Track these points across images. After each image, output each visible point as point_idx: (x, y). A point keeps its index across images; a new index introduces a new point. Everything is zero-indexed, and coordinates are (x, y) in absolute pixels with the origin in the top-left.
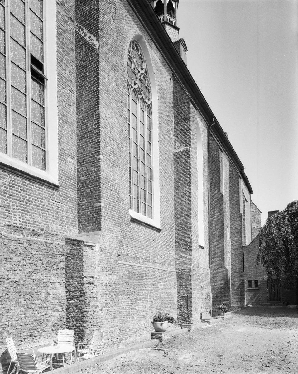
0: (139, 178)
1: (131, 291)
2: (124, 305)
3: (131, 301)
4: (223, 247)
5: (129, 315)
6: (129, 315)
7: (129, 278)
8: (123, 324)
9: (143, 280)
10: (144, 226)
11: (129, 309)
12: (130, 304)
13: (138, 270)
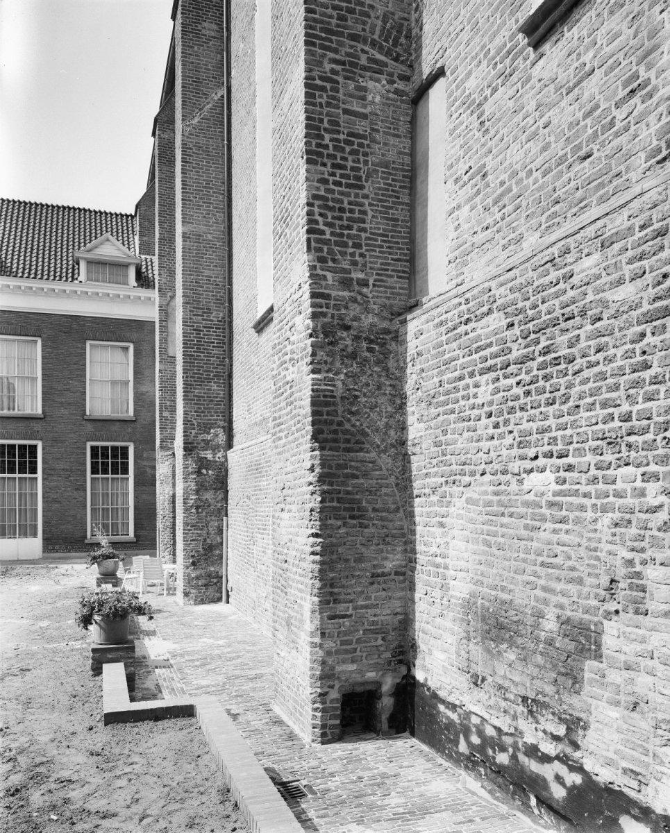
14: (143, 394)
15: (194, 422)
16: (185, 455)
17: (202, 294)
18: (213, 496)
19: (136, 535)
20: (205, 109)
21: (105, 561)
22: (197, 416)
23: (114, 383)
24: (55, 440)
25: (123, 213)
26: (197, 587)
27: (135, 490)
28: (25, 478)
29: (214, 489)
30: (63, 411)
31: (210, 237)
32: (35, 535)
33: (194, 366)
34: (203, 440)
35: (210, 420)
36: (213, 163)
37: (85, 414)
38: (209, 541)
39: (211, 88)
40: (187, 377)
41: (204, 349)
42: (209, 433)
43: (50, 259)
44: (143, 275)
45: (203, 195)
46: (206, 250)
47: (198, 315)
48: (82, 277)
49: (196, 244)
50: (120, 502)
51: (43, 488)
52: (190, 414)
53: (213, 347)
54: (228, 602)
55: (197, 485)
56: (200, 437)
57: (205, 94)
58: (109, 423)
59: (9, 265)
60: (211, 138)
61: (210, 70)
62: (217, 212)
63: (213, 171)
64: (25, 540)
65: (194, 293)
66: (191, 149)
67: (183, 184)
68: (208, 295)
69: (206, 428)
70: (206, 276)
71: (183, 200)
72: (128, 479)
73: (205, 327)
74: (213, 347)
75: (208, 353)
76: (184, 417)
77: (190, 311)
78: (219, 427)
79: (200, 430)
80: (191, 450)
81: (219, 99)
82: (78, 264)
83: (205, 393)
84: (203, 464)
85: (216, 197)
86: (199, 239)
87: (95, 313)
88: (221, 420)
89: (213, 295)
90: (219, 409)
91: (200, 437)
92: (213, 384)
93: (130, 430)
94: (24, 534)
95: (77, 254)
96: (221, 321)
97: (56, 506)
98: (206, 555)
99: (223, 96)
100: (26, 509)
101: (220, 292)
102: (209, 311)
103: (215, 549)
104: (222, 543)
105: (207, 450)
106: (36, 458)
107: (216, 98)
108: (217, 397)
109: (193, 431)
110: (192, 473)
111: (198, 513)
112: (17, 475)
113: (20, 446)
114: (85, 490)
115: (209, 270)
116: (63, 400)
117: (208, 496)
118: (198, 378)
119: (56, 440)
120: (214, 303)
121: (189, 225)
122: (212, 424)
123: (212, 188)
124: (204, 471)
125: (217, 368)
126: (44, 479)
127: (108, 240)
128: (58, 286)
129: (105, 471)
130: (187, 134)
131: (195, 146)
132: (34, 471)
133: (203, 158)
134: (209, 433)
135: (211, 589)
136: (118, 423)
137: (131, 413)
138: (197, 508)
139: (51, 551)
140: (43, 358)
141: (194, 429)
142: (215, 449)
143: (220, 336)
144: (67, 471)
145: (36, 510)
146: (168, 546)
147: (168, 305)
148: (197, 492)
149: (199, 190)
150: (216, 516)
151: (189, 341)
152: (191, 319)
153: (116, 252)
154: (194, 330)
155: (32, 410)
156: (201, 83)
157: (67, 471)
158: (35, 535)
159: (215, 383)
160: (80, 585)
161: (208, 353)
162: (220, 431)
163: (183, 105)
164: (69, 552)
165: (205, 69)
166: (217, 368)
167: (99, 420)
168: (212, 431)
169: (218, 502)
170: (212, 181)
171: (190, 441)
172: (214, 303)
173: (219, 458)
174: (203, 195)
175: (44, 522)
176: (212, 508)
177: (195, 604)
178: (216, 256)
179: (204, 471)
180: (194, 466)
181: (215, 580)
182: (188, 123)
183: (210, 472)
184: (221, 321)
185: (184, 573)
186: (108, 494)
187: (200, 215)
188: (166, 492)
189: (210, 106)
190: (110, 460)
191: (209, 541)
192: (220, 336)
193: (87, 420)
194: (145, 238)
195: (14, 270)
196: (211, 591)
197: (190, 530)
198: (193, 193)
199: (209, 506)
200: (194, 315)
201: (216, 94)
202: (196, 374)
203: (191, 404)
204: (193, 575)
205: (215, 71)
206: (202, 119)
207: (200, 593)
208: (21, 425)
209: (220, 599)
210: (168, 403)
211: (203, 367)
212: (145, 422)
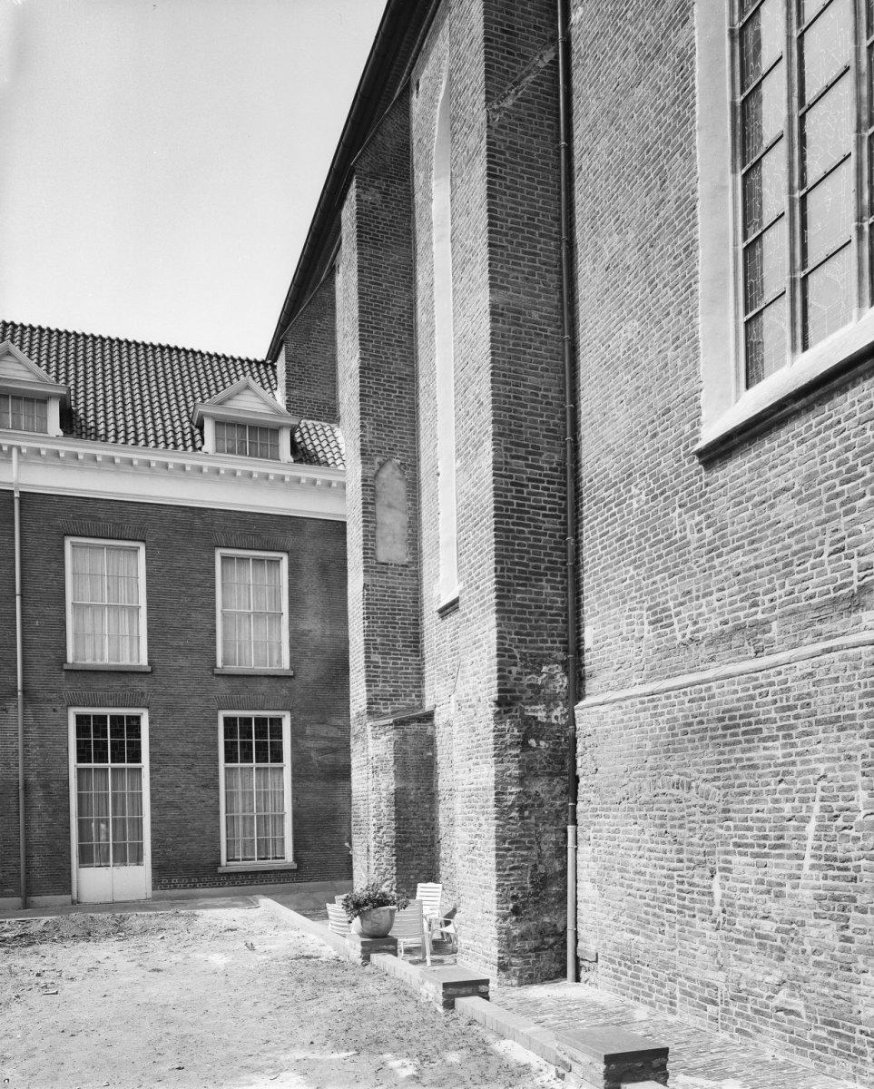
0: (796, 93)
1: (684, 804)
2: (644, 861)
3: (680, 851)
4: (223, 579)
5: (669, 911)
6: (669, 911)
7: (670, 749)
8: (642, 940)
9: (764, 740)
10: (808, 408)
11: (668, 881)
12: (676, 865)
13: (727, 696)
14: (304, 634)
15: (516, 652)
16: (497, 714)
17: (525, 420)
18: (545, 788)
19: (296, 858)
20: (523, 84)
21: (374, 911)
22: (520, 641)
23: (258, 616)
24: (170, 708)
25: (251, 358)
26: (521, 954)
27: (294, 788)
28: (123, 769)
29: (550, 774)
30: (182, 662)
31: (535, 315)
32: (138, 860)
33: (513, 551)
34: (531, 686)
35: (541, 649)
36: (539, 183)
37: (215, 666)
38: (541, 869)
39: (533, 47)
40: (502, 570)
41: (530, 519)
42: (539, 673)
43: (154, 420)
44: (299, 447)
45: (524, 238)
46: (531, 340)
47: (518, 457)
48: (209, 445)
49: (513, 328)
50: (270, 805)
51: (152, 785)
52: (508, 637)
53: (545, 516)
54: (578, 979)
55: (520, 767)
56: (526, 680)
57: (522, 56)
58: (254, 679)
59: (92, 424)
60: (535, 136)
61: (530, 13)
62: (547, 271)
63: (539, 196)
64: (123, 869)
65: (511, 417)
66: (502, 153)
67: (490, 217)
68: (535, 422)
69: (535, 663)
70: (530, 387)
71: (490, 245)
72: (282, 769)
73: (530, 480)
74: (545, 516)
75: (535, 527)
76: (499, 644)
77: (506, 449)
78: (556, 662)
79: (525, 667)
80: (511, 704)
81: (546, 67)
82: (201, 427)
83: (531, 600)
84: (531, 729)
85: (545, 243)
86: (518, 319)
87: (226, 504)
88: (559, 650)
89: (542, 422)
90: (555, 628)
91: (526, 680)
92: (544, 583)
93: (284, 691)
94: (121, 859)
95: (201, 409)
96: (555, 470)
97: (171, 814)
98: (536, 894)
99: (555, 62)
100: (124, 820)
101: (553, 417)
102: (536, 452)
103: (551, 884)
104: (564, 873)
105: (536, 704)
106: (139, 736)
107: (541, 65)
108: (551, 608)
109: (514, 670)
110: (512, 746)
111: (522, 818)
112: (109, 765)
113: (112, 717)
114: (217, 787)
115: (535, 375)
116: (182, 643)
117: (539, 786)
118: (520, 571)
119: (170, 708)
120: (544, 436)
121: (502, 292)
122: (544, 656)
123: (537, 227)
124: (532, 742)
125: (550, 555)
126: (152, 771)
127: (248, 387)
128: (173, 458)
129: (247, 758)
130: (495, 125)
131: (509, 148)
132: (136, 757)
133: (523, 171)
134: (539, 673)
135: (545, 955)
136: (266, 681)
137: (286, 664)
138: (522, 809)
139: (165, 887)
140: (149, 575)
141: (515, 665)
142: (551, 701)
143: (554, 496)
144: (188, 756)
145: (140, 821)
146: (388, 876)
147: (376, 476)
148: (521, 780)
149: (517, 230)
150: (552, 824)
151: (505, 503)
152: (507, 463)
153: (264, 407)
154: (512, 484)
155: (131, 660)
156: (516, 35)
157: (188, 756)
158: (138, 860)
159: (548, 581)
160: (293, 953)
161: (535, 527)
162: (557, 669)
163: (486, 72)
164: (195, 887)
165: (523, 11)
166: (550, 555)
167: (244, 676)
168: (545, 669)
169: (554, 798)
170: (538, 214)
171: (508, 687)
172: (544, 436)
173: (556, 718)
174: (524, 238)
175: (154, 840)
176: (546, 810)
177: (520, 985)
178: (546, 351)
179: (532, 742)
180: (516, 733)
181: (551, 940)
182: (496, 107)
183: (542, 743)
184: (555, 470)
185: (501, 928)
186: (251, 793)
187: (520, 275)
188: (383, 786)
189: (531, 78)
190: (254, 740)
191: (541, 869)
192: (554, 496)
193: (218, 675)
194: (295, 392)
195: (102, 432)
196: (546, 962)
197: (509, 850)
198: (506, 234)
199: (541, 805)
200: (513, 457)
201: (541, 57)
202: (517, 564)
203: (509, 619)
204: (516, 932)
205: (537, 16)
206: (519, 99)
207: (528, 963)
208: (116, 684)
209: (562, 974)
210: (379, 640)
211: (528, 552)
212: (309, 679)
